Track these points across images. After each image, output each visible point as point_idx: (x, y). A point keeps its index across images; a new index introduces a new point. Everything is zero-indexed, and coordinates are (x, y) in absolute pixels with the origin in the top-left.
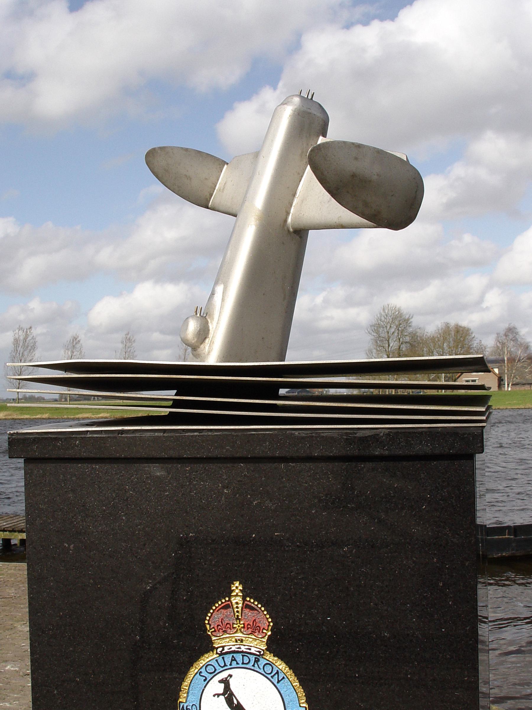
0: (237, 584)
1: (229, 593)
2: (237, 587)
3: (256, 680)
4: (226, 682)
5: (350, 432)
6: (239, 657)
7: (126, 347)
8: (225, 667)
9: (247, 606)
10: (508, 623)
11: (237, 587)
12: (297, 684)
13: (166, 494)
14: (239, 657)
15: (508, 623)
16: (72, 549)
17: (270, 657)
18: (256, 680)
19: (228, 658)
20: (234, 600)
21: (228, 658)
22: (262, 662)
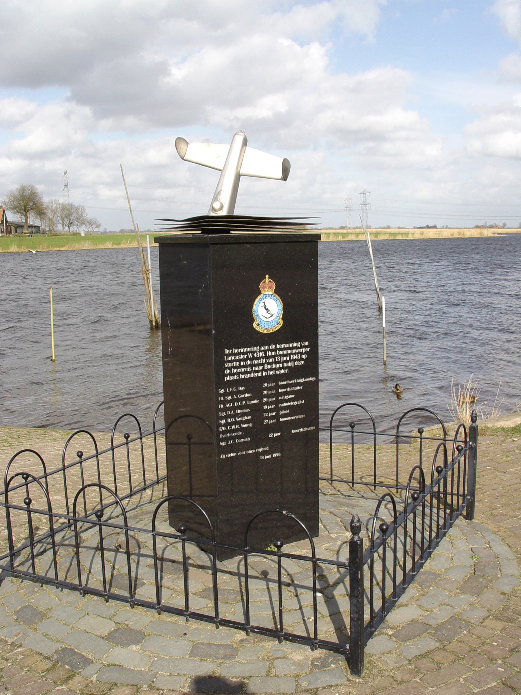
0: (267, 275)
1: (265, 278)
2: (267, 276)
3: (185, 634)
4: (264, 302)
5: (290, 402)
6: (267, 295)
7: (339, 683)
8: (264, 298)
9: (270, 282)
10: (18, 420)
11: (267, 276)
12: (281, 301)
13: (246, 549)
14: (267, 295)
15: (18, 420)
16: (244, 452)
17: (275, 294)
18: (185, 634)
19: (265, 296)
20: (266, 280)
21: (265, 296)
22: (273, 296)
